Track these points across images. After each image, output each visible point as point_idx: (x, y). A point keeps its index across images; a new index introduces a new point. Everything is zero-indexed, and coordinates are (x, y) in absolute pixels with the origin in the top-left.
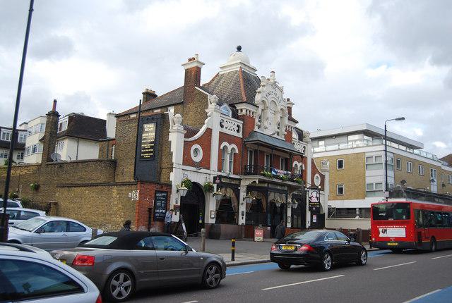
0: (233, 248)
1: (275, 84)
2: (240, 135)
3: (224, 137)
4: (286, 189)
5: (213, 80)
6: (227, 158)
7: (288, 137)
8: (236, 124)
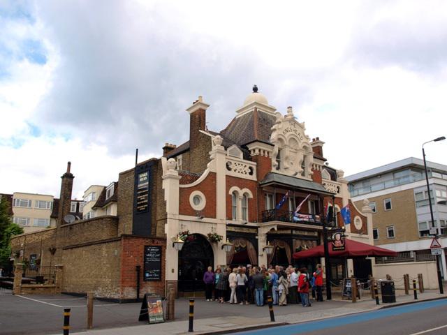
0: (190, 315)
1: (293, 121)
2: (254, 177)
3: (231, 181)
4: (316, 234)
5: (230, 125)
6: (239, 204)
7: (317, 176)
8: (248, 166)
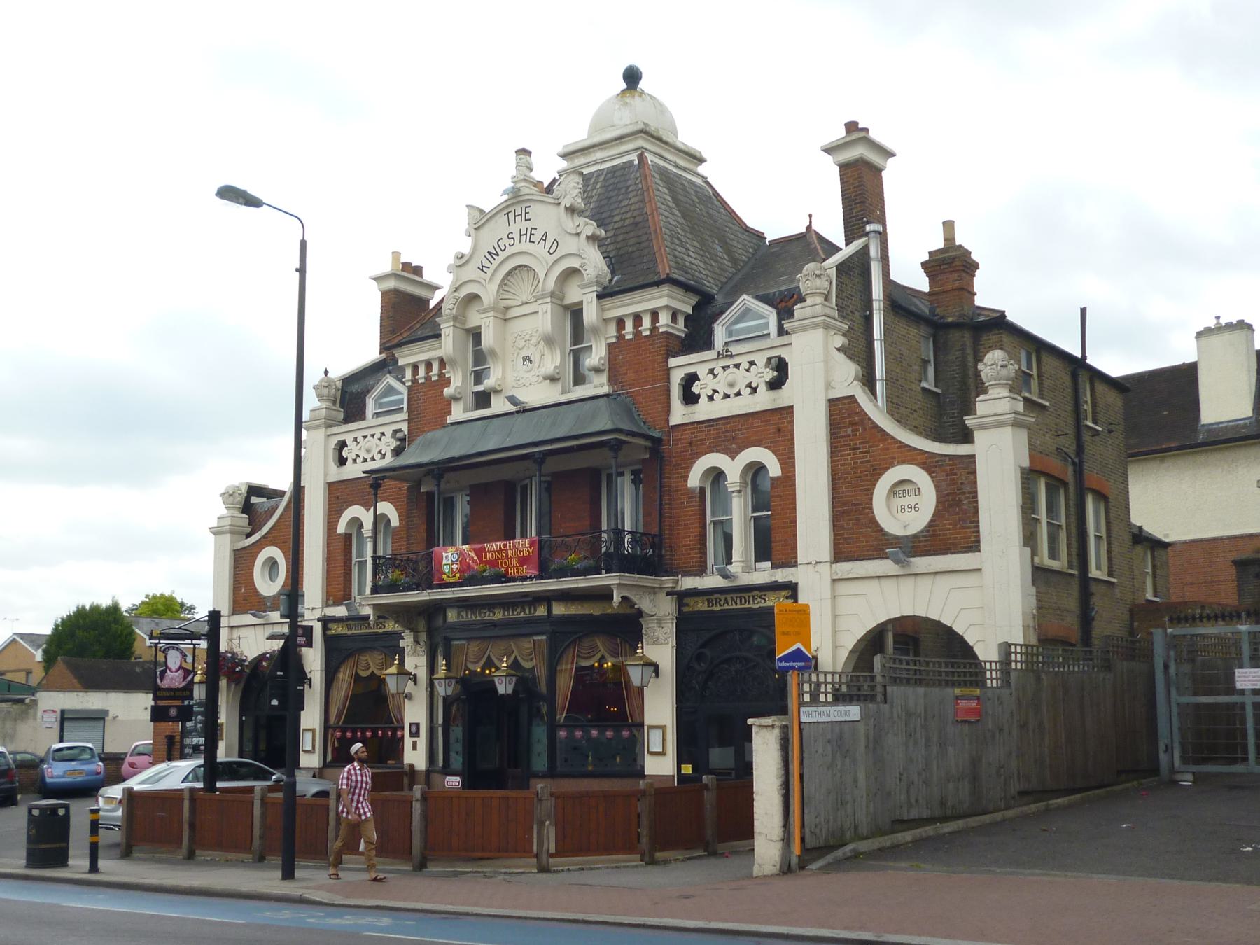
8: (761, 359)
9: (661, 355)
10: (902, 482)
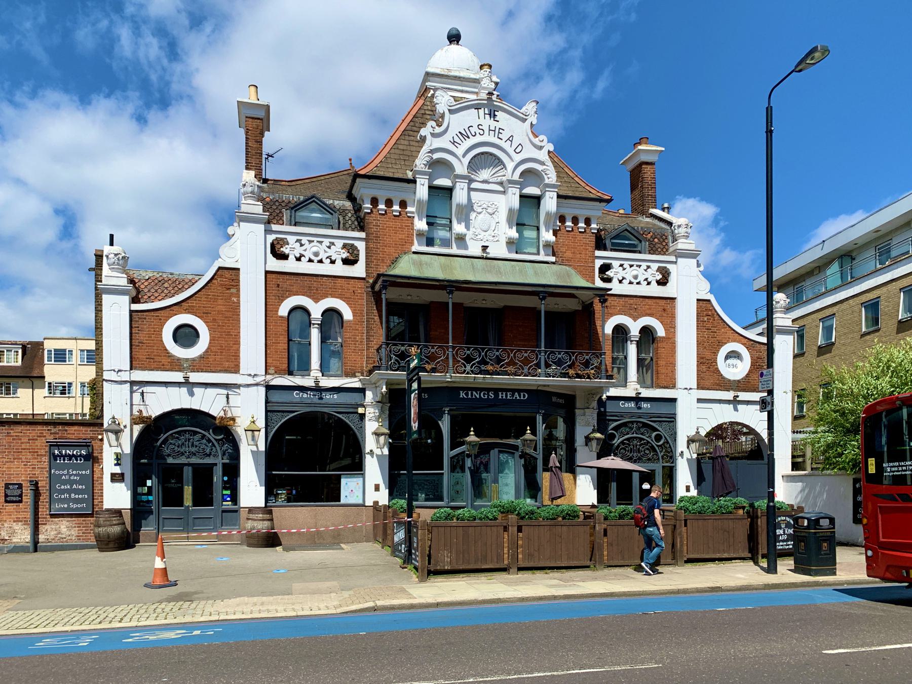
8: (655, 266)
9: (591, 246)
10: (733, 352)
